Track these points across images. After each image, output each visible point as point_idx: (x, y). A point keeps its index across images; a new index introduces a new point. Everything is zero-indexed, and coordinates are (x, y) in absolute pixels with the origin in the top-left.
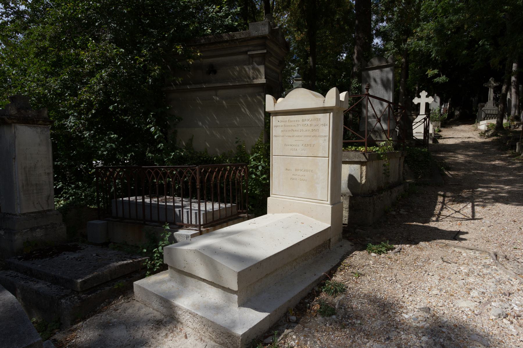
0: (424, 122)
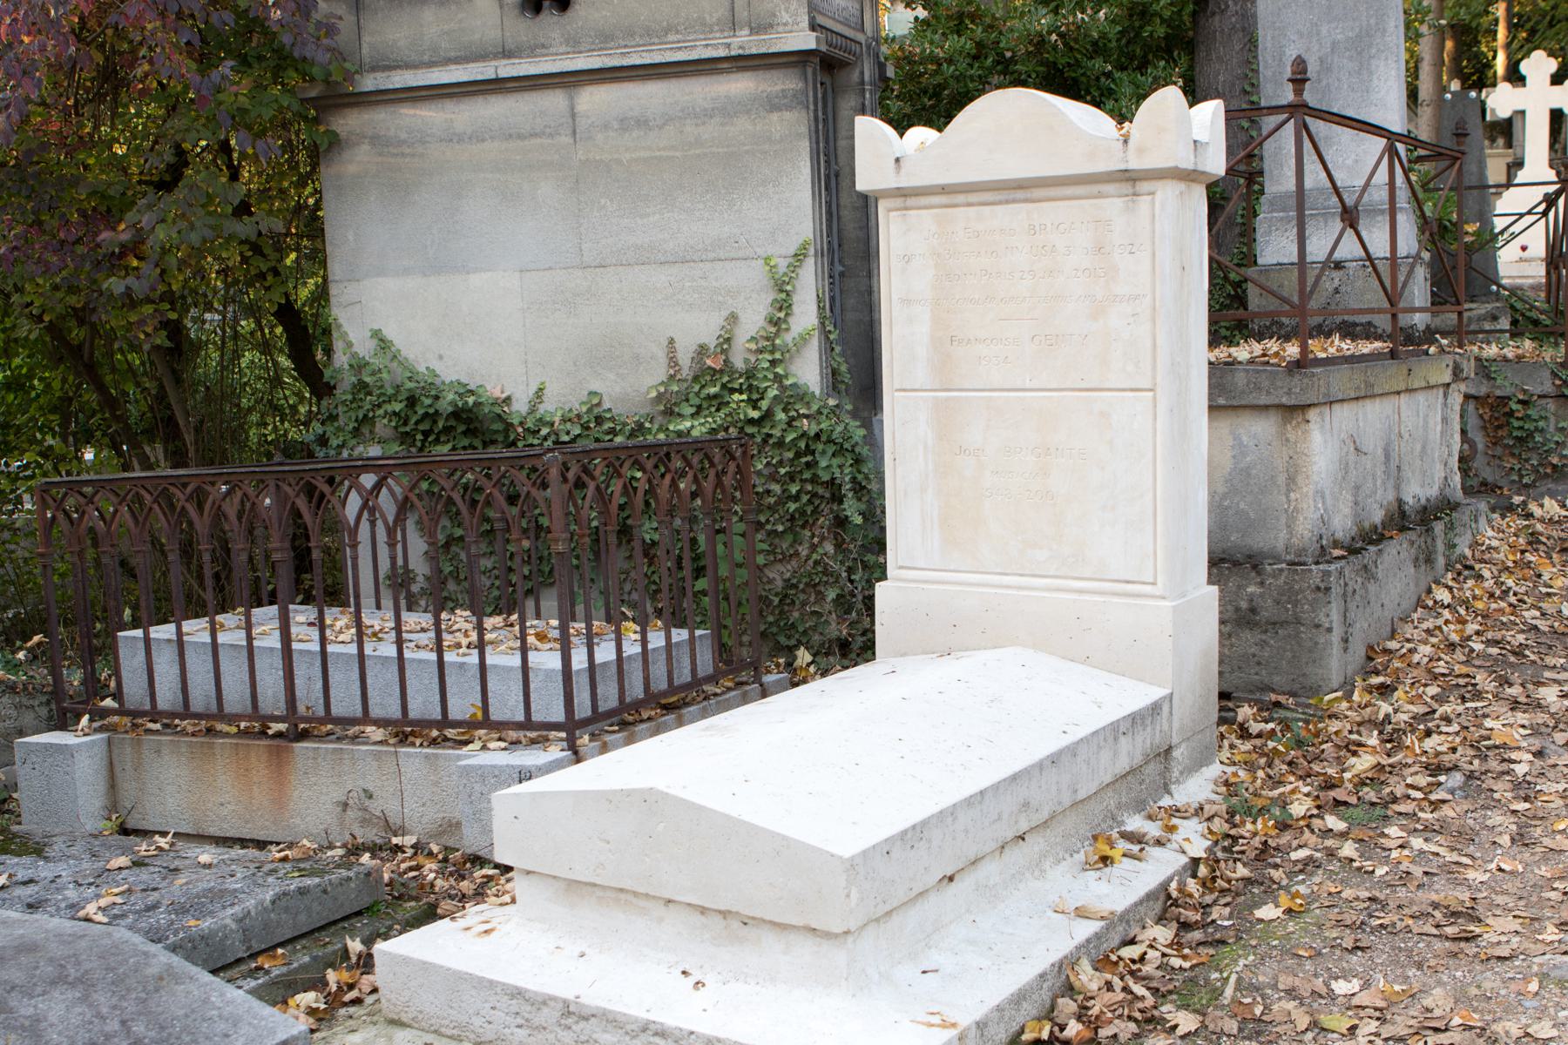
0: (1545, 214)
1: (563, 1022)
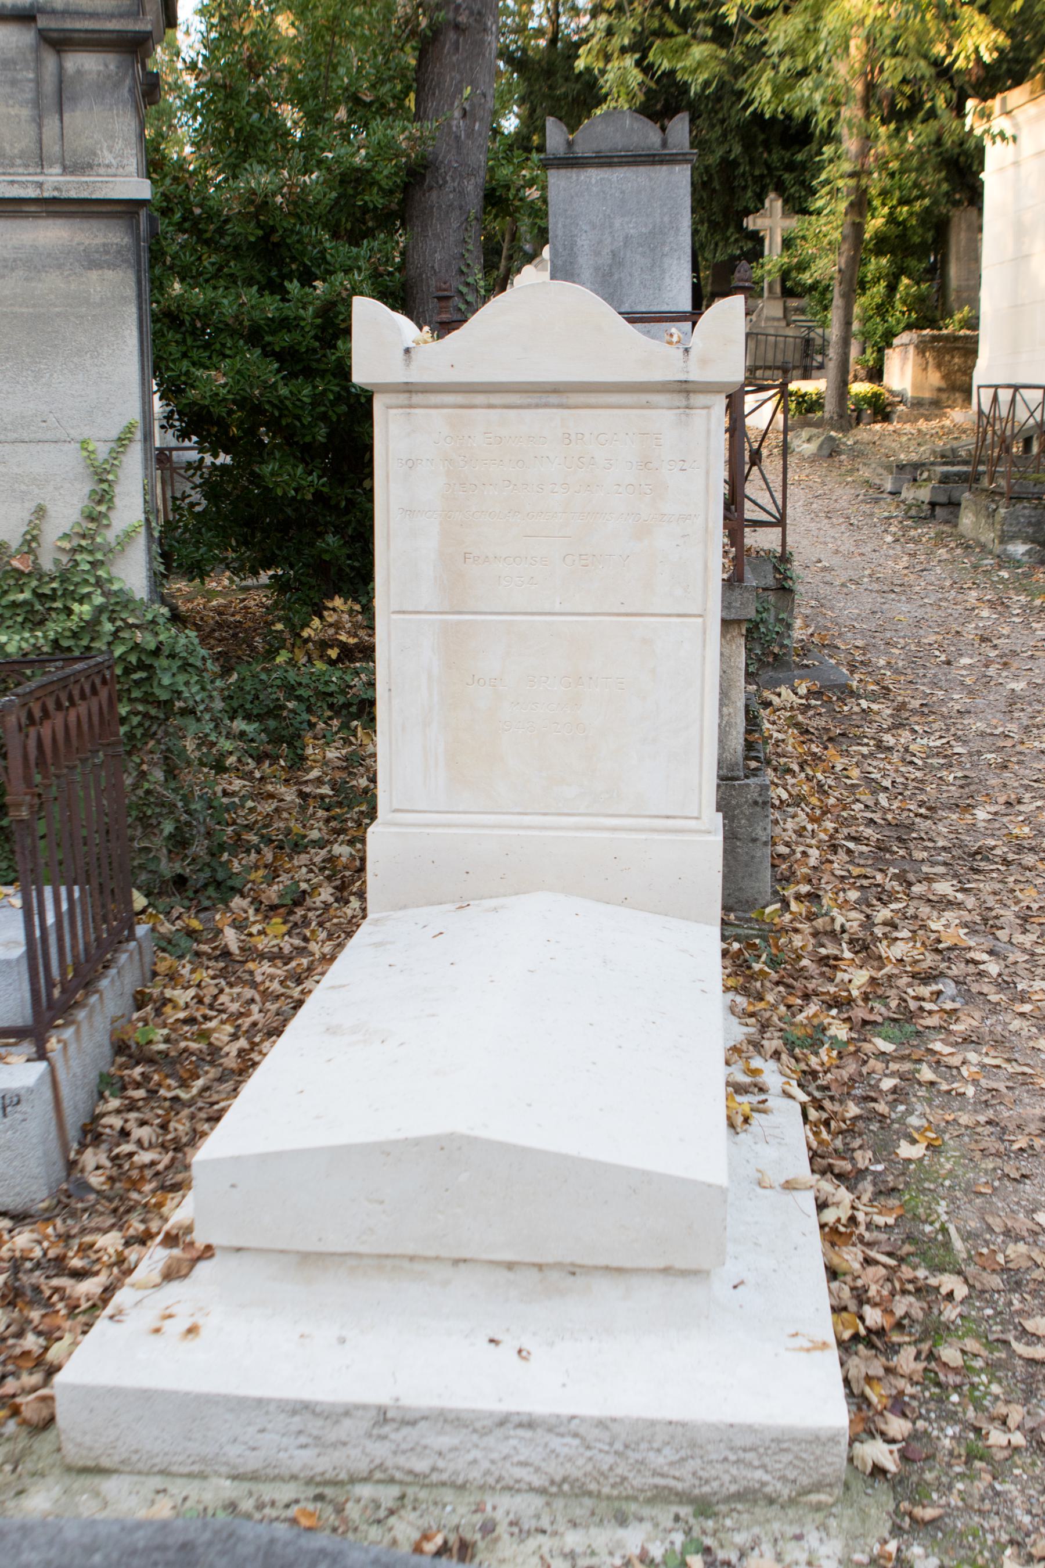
1: (375, 1432)
